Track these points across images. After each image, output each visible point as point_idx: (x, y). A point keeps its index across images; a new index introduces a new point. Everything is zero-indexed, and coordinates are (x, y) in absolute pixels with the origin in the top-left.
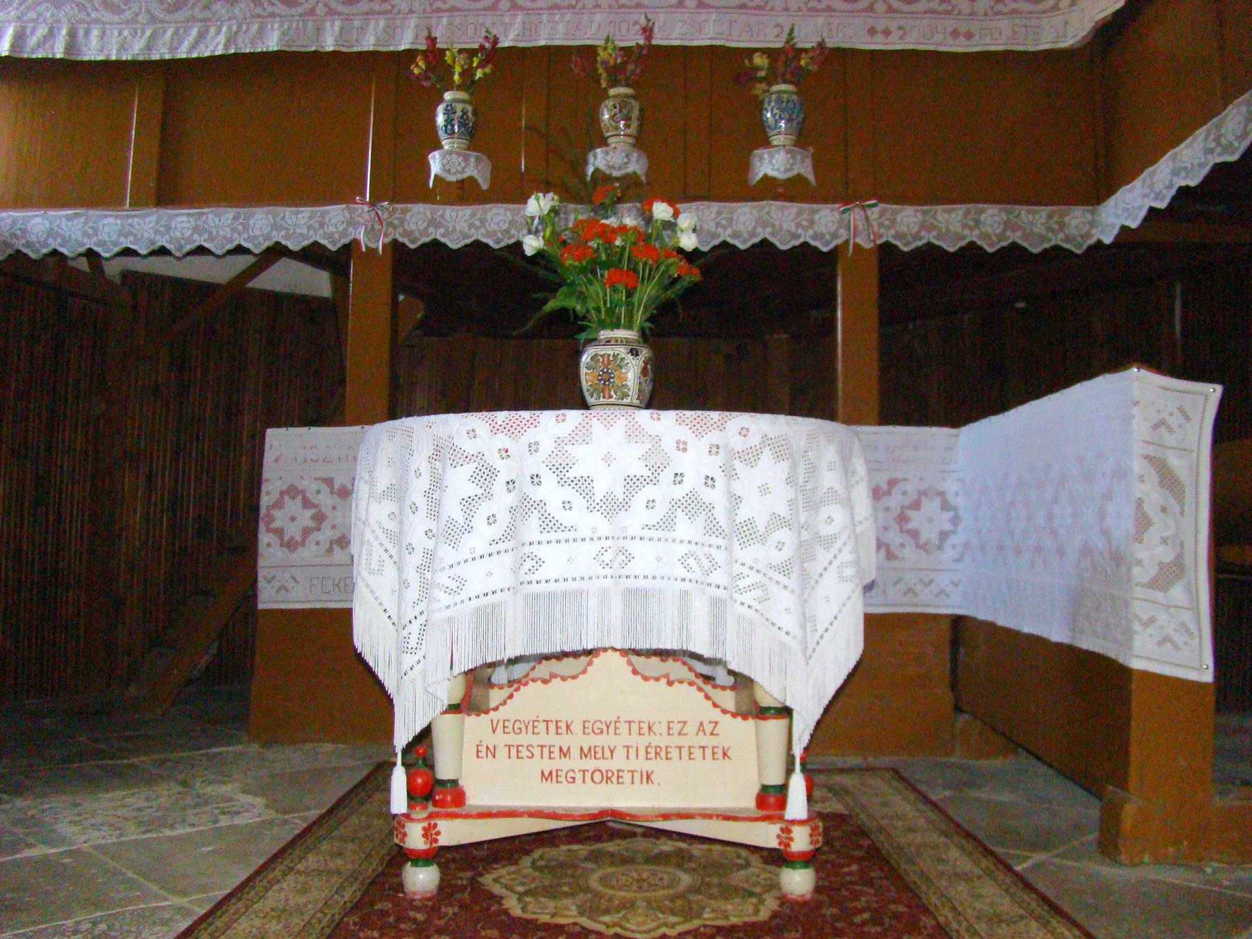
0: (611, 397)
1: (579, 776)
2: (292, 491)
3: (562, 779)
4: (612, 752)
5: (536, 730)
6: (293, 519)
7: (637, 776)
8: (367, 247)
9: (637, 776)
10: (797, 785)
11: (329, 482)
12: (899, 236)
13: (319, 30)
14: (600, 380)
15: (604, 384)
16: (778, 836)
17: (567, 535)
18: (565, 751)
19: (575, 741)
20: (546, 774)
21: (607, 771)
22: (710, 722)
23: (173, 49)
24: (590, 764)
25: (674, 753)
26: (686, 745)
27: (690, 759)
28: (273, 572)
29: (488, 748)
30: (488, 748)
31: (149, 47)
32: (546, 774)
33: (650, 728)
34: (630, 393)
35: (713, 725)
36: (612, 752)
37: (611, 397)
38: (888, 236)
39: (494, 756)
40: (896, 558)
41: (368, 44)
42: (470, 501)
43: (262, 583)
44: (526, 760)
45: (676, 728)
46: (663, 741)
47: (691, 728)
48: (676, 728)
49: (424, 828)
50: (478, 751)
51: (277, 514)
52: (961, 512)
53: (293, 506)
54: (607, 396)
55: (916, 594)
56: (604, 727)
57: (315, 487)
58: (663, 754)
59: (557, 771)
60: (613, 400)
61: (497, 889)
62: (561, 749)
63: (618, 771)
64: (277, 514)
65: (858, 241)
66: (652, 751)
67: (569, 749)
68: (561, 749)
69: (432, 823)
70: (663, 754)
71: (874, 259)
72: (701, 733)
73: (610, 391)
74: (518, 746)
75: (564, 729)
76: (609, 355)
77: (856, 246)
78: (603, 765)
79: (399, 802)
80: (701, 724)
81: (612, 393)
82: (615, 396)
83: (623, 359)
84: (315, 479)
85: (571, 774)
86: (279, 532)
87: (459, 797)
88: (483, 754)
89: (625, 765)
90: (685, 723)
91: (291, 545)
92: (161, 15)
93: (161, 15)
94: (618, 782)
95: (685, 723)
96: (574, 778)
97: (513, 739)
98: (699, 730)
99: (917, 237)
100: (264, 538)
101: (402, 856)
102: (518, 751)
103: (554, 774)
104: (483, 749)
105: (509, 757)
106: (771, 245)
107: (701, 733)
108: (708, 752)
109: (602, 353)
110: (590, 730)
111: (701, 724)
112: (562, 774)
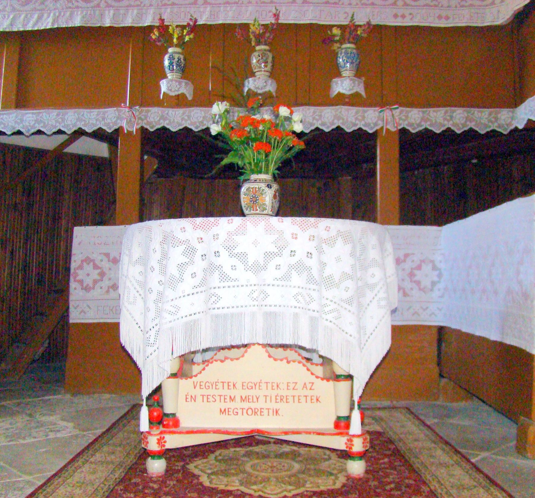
0: (257, 210)
1: (240, 412)
2: (87, 260)
3: (231, 413)
4: (257, 399)
6: (88, 275)
7: (271, 411)
8: (127, 130)
9: (271, 411)
11: (107, 255)
12: (410, 125)
13: (102, 15)
14: (251, 201)
16: (346, 443)
17: (234, 283)
19: (238, 393)
20: (223, 410)
23: (25, 25)
24: (246, 405)
25: (291, 399)
27: (299, 402)
29: (191, 396)
30: (191, 396)
31: (12, 24)
34: (267, 208)
35: (311, 384)
36: (257, 399)
37: (257, 210)
38: (404, 125)
39: (195, 401)
40: (408, 296)
41: (128, 22)
42: (182, 265)
44: (212, 403)
45: (291, 386)
46: (284, 393)
47: (300, 386)
48: (291, 386)
49: (158, 439)
51: (80, 272)
53: (89, 268)
55: (419, 315)
57: (100, 258)
58: (285, 400)
59: (228, 409)
60: (258, 212)
61: (196, 472)
62: (230, 397)
63: (261, 409)
64: (80, 272)
65: (388, 127)
66: (279, 398)
68: (230, 397)
69: (162, 436)
70: (285, 400)
72: (305, 389)
73: (256, 207)
74: (208, 396)
76: (256, 188)
77: (387, 130)
78: (253, 405)
79: (144, 425)
80: (305, 384)
81: (258, 208)
82: (259, 210)
84: (100, 254)
85: (236, 410)
86: (81, 282)
87: (176, 423)
88: (189, 400)
90: (296, 383)
92: (18, 7)
93: (18, 7)
95: (296, 383)
97: (205, 392)
98: (304, 387)
99: (419, 125)
100: (73, 285)
101: (146, 454)
102: (208, 398)
103: (227, 410)
104: (189, 397)
106: (342, 129)
107: (305, 389)
108: (309, 399)
109: (252, 187)
111: (305, 384)
112: (231, 410)
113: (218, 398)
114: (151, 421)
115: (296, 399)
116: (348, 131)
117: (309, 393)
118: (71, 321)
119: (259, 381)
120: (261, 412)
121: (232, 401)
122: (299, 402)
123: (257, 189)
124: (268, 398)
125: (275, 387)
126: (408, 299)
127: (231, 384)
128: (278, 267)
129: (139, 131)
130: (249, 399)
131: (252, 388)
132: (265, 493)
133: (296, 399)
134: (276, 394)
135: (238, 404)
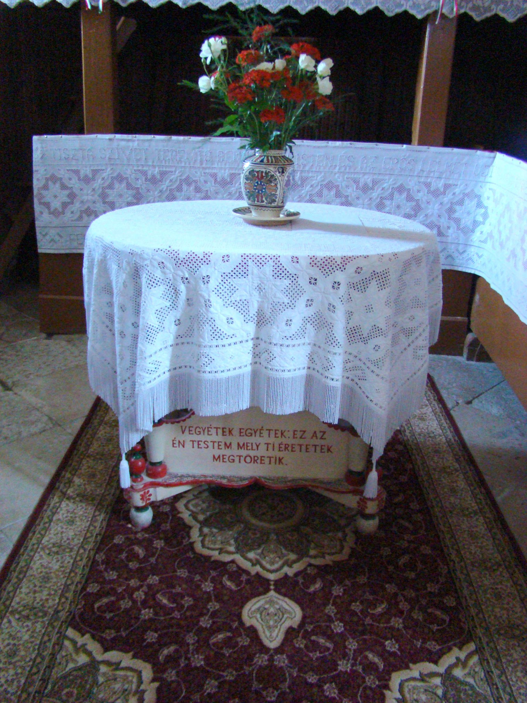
0: (263, 201)
1: (237, 459)
2: (54, 179)
3: (226, 460)
4: (258, 446)
5: (210, 433)
6: (56, 196)
7: (273, 460)
8: (92, 6)
9: (273, 460)
10: (373, 476)
11: (77, 172)
14: (255, 189)
15: (258, 192)
16: (358, 503)
17: (230, 341)
18: (228, 445)
20: (216, 457)
21: (254, 457)
22: (321, 432)
24: (243, 452)
25: (297, 448)
26: (305, 444)
27: (307, 451)
28: (46, 230)
29: (179, 442)
30: (179, 442)
32: (216, 457)
33: (282, 434)
34: (277, 200)
35: (322, 434)
36: (258, 446)
37: (263, 201)
39: (183, 447)
40: (444, 236)
42: (162, 310)
43: (39, 237)
44: (203, 449)
45: (299, 434)
46: (291, 441)
47: (308, 435)
48: (299, 434)
49: (142, 495)
50: (173, 444)
52: (489, 211)
53: (55, 188)
54: (260, 200)
55: (453, 259)
56: (253, 432)
57: (67, 176)
58: (290, 448)
59: (223, 456)
60: (264, 204)
62: (225, 444)
63: (261, 457)
65: (444, 11)
66: (283, 446)
67: (230, 444)
68: (225, 444)
69: (146, 491)
70: (290, 448)
71: (452, 29)
72: (314, 438)
73: (262, 198)
74: (198, 441)
75: (227, 433)
76: (262, 172)
78: (252, 453)
79: (126, 481)
80: (315, 432)
81: (264, 199)
82: (265, 201)
83: (272, 176)
84: (68, 170)
85: (231, 458)
87: (164, 472)
88: (177, 445)
89: (266, 454)
90: (304, 432)
91: (56, 213)
94: (261, 463)
95: (304, 432)
96: (234, 460)
97: (195, 437)
98: (313, 436)
100: (37, 208)
102: (199, 444)
103: (221, 458)
104: (177, 443)
105: (193, 447)
106: (382, 13)
107: (314, 438)
108: (318, 449)
109: (257, 170)
110: (244, 434)
111: (315, 432)
112: (227, 457)
113: (210, 445)
114: (134, 473)
115: (304, 448)
116: (390, 14)
117: (319, 442)
118: (40, 251)
119: (260, 427)
120: (261, 460)
121: (228, 447)
122: (307, 451)
123: (264, 175)
124: (271, 447)
125: (279, 435)
126: (444, 239)
127: (227, 430)
128: (288, 323)
129: (109, 6)
130: (247, 446)
131: (251, 435)
132: (264, 632)
133: (304, 448)
134: (280, 442)
135: (235, 451)
